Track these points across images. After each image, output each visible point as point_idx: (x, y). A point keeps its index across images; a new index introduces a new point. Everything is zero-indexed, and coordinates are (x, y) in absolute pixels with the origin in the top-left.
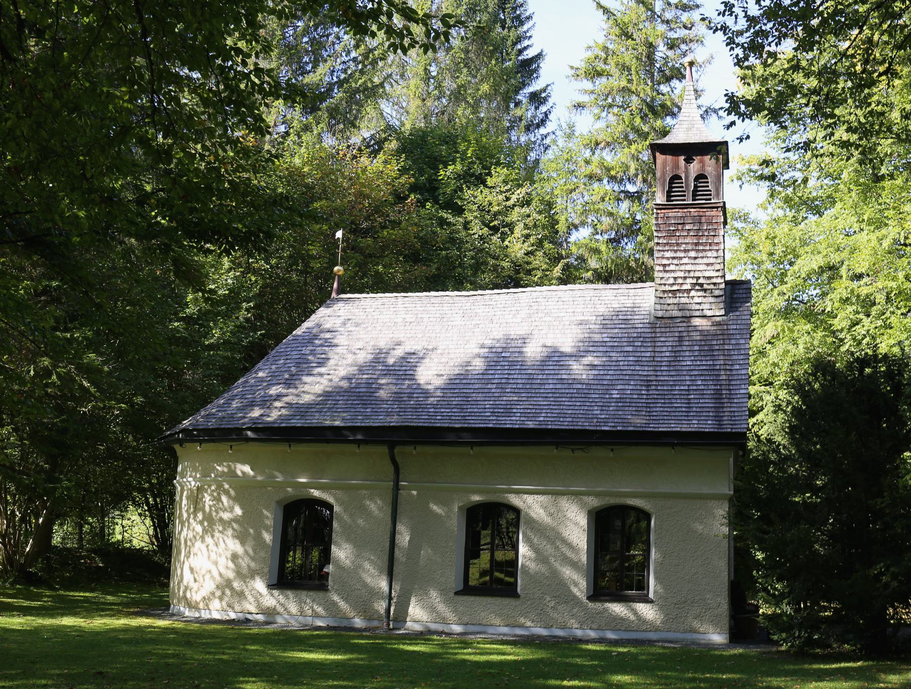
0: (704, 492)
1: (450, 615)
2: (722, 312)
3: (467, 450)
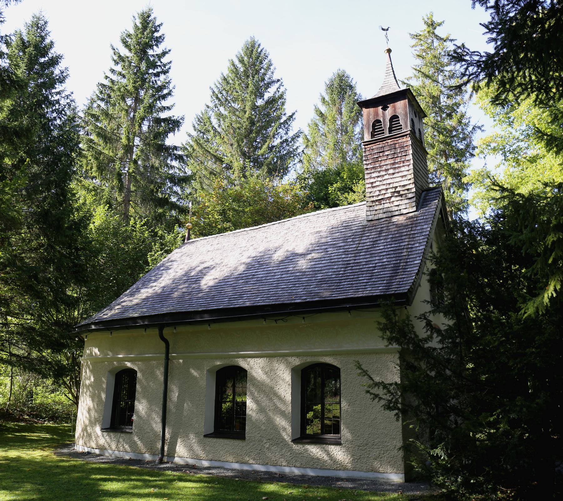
0: (379, 347)
1: (202, 454)
2: (415, 209)
3: (206, 327)
